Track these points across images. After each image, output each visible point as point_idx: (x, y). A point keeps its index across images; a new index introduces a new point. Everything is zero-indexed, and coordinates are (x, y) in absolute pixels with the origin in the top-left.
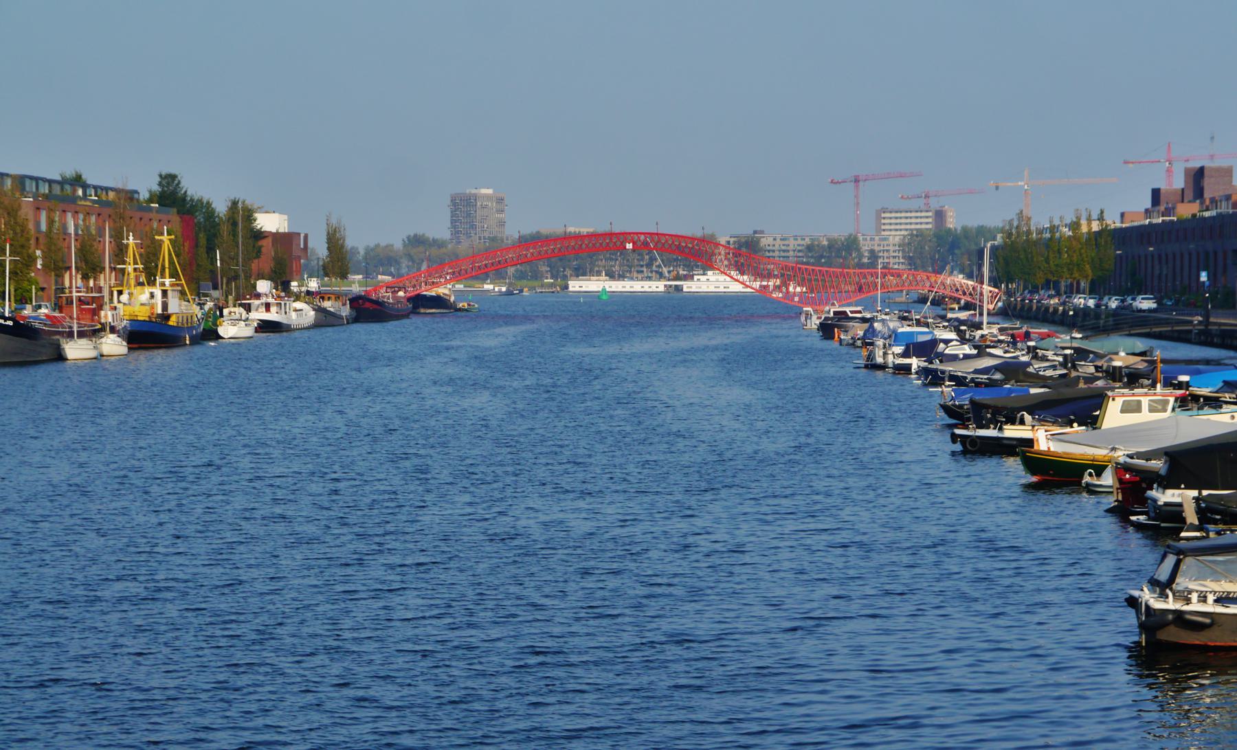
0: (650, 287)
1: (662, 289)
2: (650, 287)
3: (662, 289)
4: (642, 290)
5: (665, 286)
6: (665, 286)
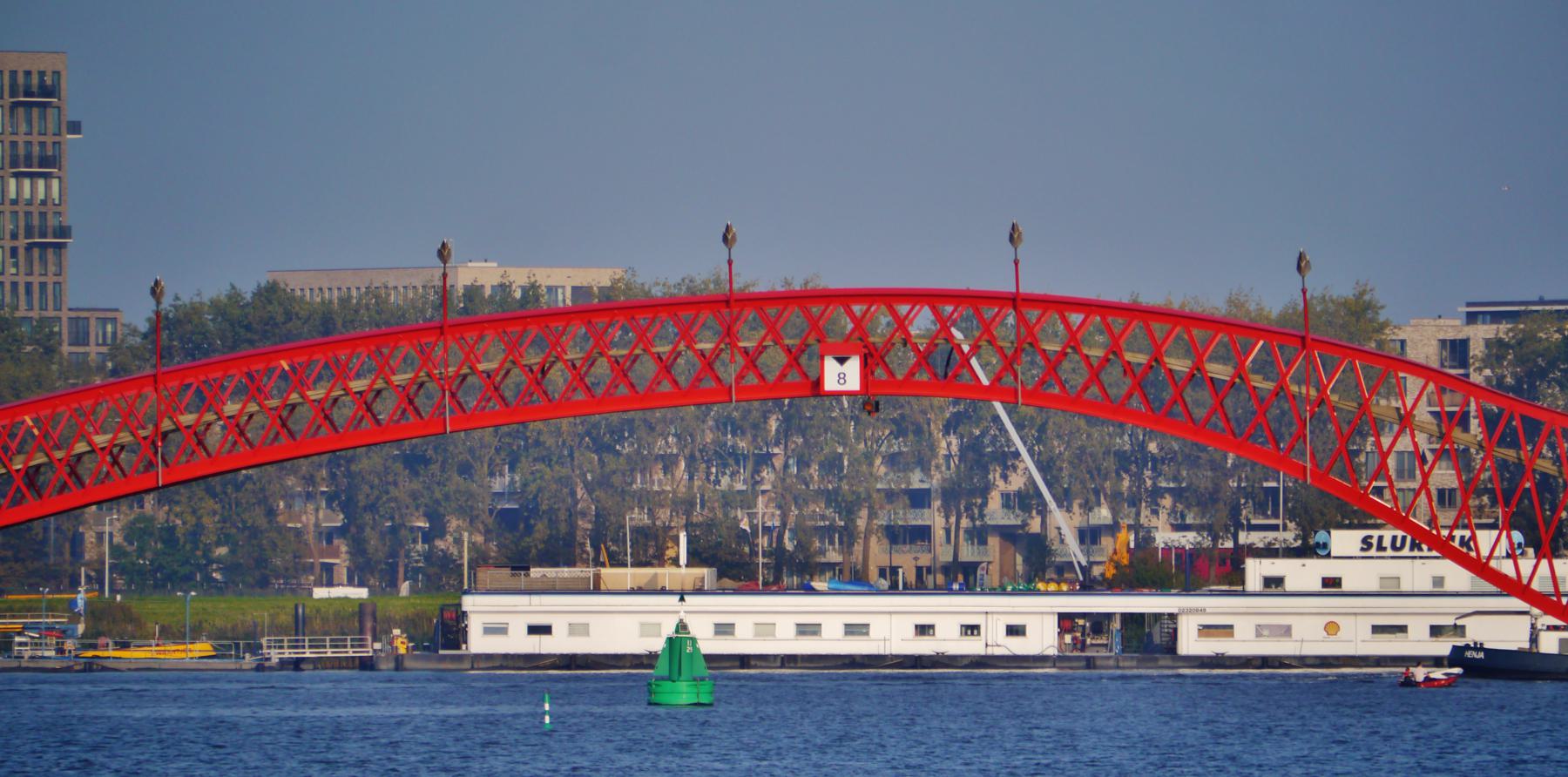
0: (971, 630)
1: (1042, 638)
2: (971, 630)
3: (1042, 638)
4: (925, 647)
5: (1066, 621)
6: (1066, 621)
